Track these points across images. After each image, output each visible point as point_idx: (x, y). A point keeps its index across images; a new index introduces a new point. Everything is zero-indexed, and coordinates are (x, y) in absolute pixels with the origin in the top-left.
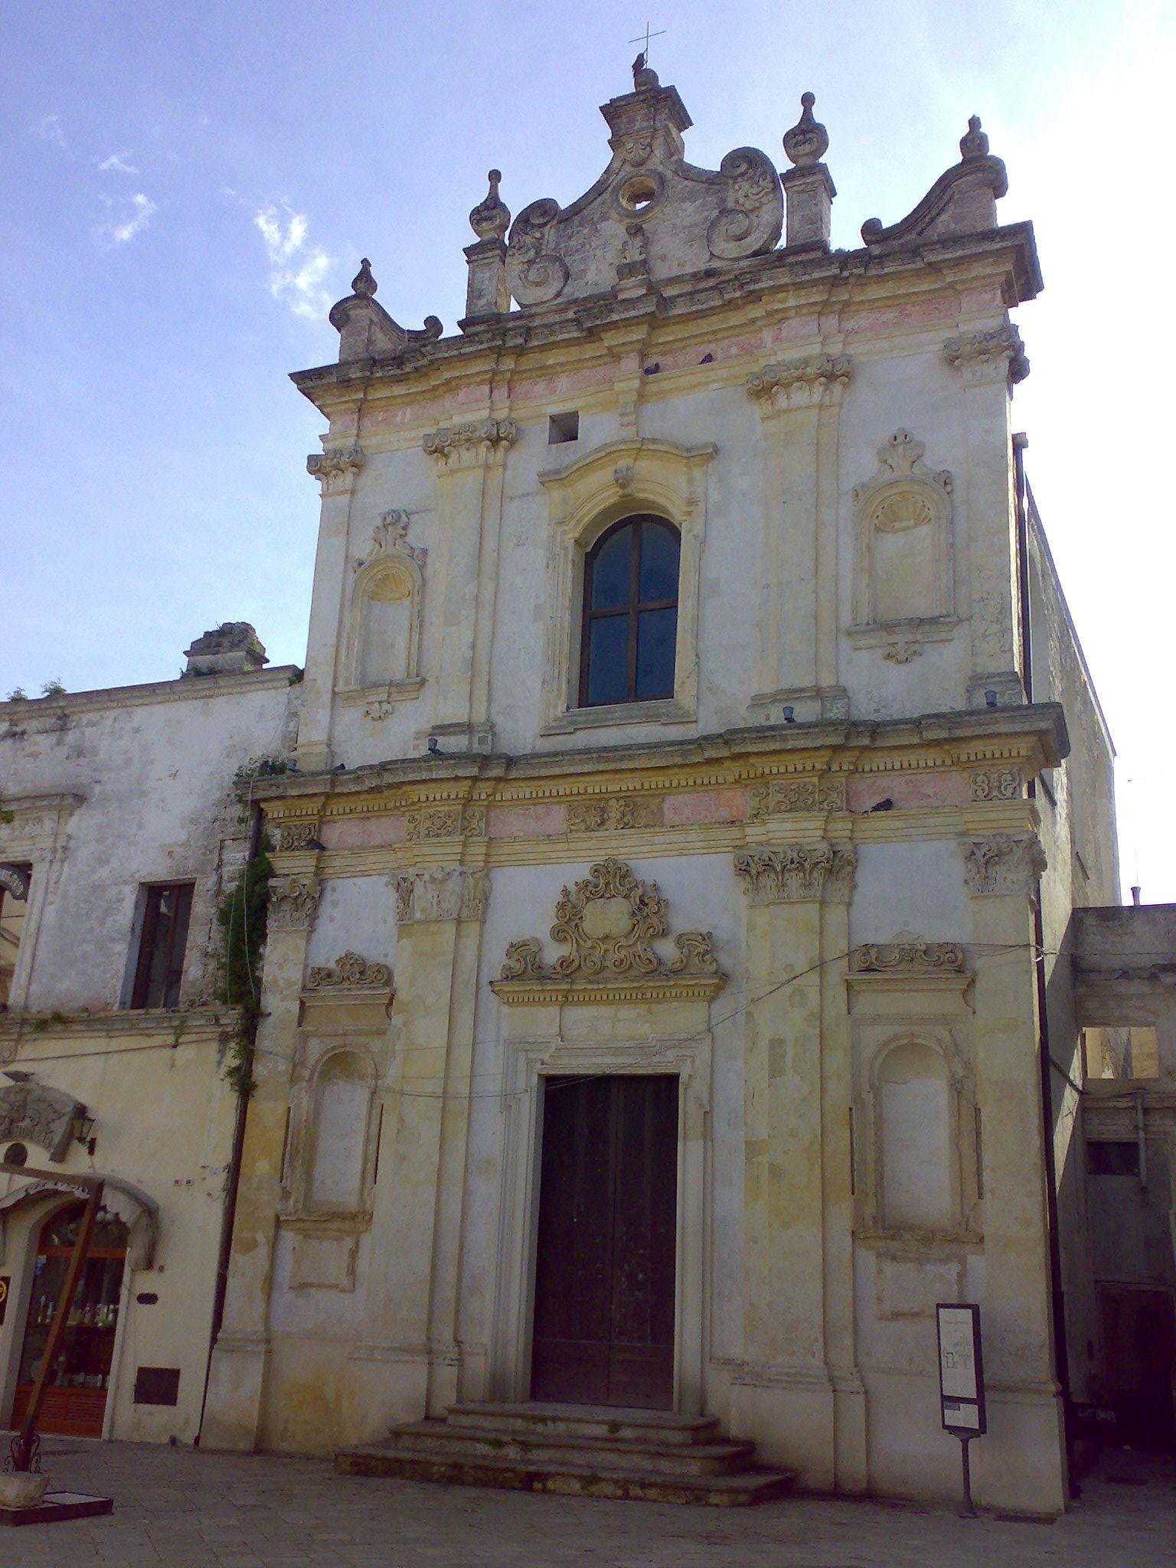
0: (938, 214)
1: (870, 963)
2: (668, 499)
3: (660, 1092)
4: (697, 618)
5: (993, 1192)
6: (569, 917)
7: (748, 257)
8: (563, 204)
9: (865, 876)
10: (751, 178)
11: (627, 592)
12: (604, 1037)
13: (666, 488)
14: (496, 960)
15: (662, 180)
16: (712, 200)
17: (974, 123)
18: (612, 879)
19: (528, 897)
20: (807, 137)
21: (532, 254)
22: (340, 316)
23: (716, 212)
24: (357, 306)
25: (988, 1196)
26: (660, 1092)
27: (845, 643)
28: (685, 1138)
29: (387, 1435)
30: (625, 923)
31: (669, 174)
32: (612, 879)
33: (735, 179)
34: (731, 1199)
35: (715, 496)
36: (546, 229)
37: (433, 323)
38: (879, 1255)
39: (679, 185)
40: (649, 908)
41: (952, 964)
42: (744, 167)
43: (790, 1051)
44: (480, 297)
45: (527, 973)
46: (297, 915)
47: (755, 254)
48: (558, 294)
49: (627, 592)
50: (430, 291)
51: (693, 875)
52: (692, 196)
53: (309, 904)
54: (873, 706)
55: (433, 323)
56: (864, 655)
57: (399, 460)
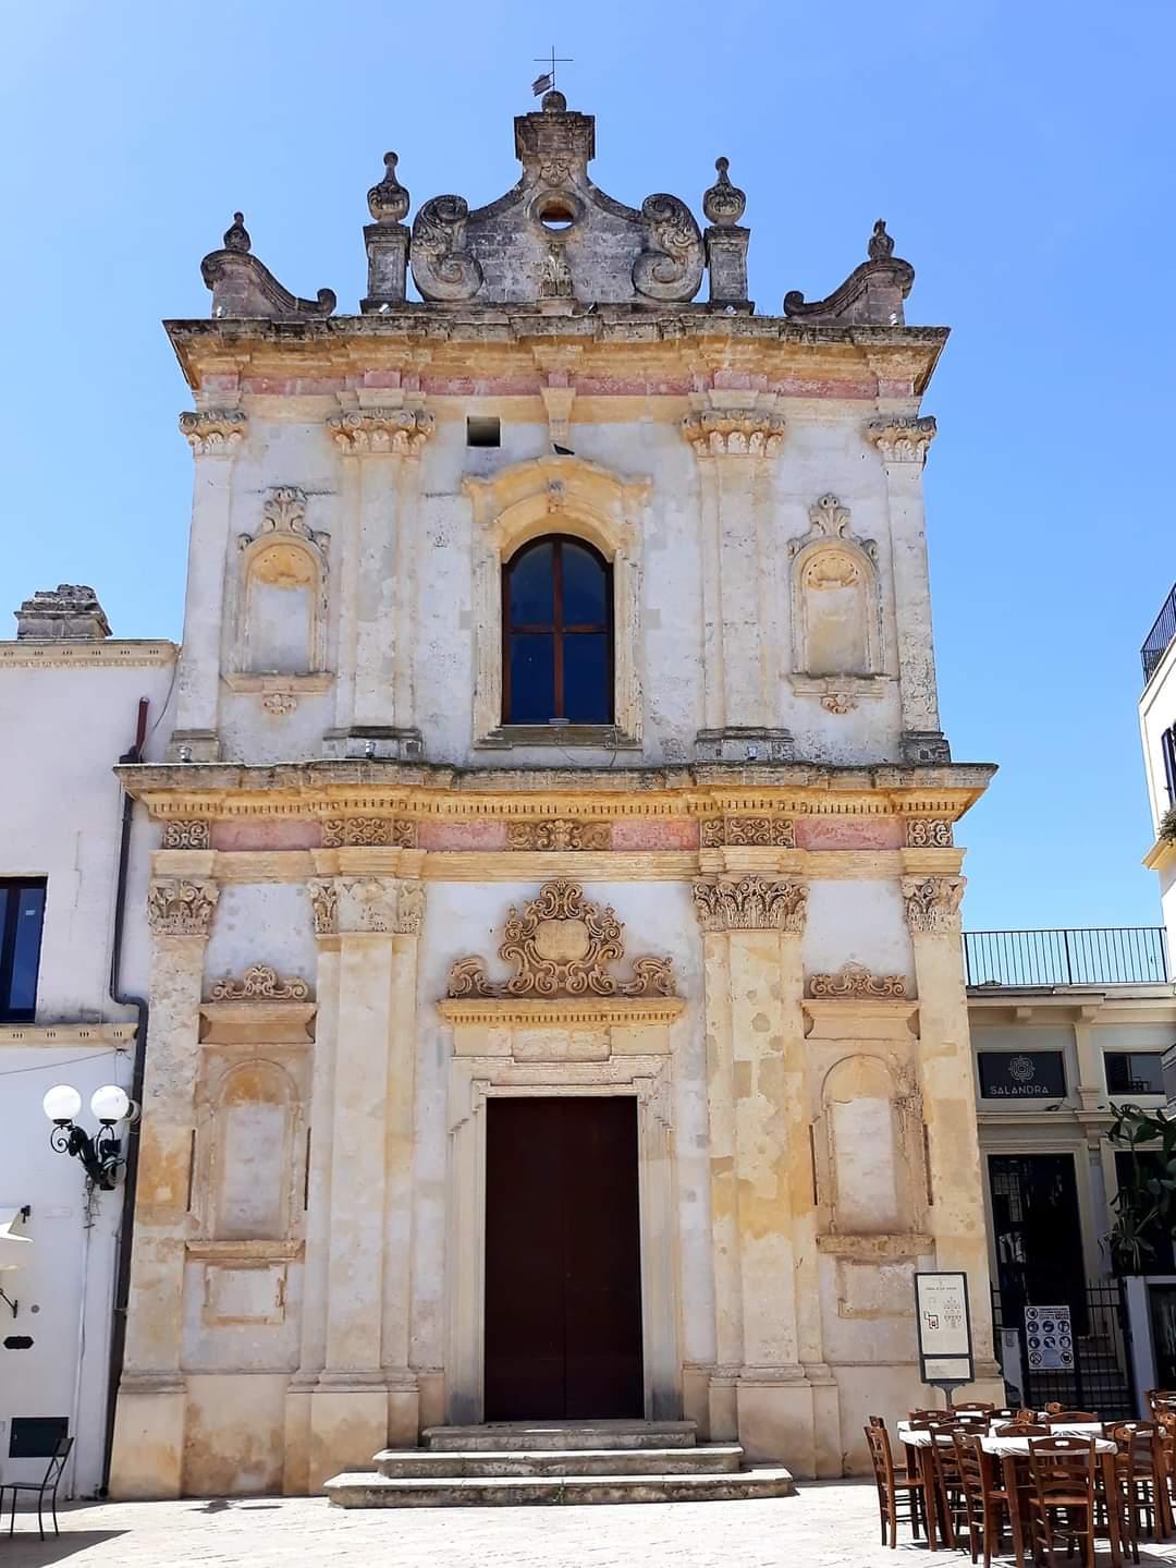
0: (854, 301)
1: (818, 989)
2: (603, 522)
3: (618, 1115)
4: (637, 649)
5: (941, 1198)
6: (519, 934)
7: (674, 301)
8: (471, 207)
9: (811, 907)
10: (676, 225)
11: (559, 630)
12: (556, 1058)
13: (602, 516)
14: (435, 973)
15: (582, 205)
16: (634, 237)
17: (880, 226)
18: (561, 902)
19: (470, 911)
20: (724, 194)
21: (443, 247)
22: (212, 268)
23: (638, 250)
24: (232, 257)
25: (937, 1201)
26: (618, 1115)
27: (786, 689)
28: (83, 1291)
29: (417, 1128)
30: (582, 947)
31: (587, 201)
32: (561, 902)
33: (658, 223)
34: (691, 1216)
35: (650, 528)
36: (456, 226)
37: (327, 296)
38: (839, 1260)
39: (598, 214)
40: (606, 934)
41: (892, 990)
42: (668, 214)
43: (755, 1072)
44: (383, 280)
45: (469, 987)
46: (190, 921)
47: (680, 300)
48: (473, 295)
49: (559, 630)
50: (322, 257)
51: (646, 903)
52: (610, 228)
53: (206, 910)
54: (816, 751)
55: (327, 296)
56: (801, 702)
57: (289, 427)
